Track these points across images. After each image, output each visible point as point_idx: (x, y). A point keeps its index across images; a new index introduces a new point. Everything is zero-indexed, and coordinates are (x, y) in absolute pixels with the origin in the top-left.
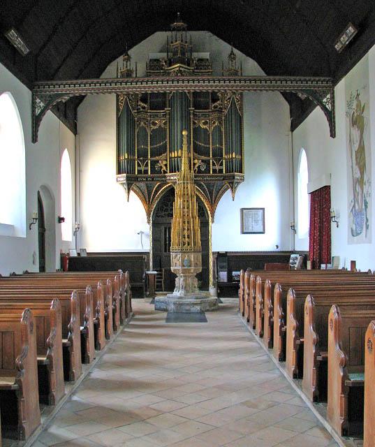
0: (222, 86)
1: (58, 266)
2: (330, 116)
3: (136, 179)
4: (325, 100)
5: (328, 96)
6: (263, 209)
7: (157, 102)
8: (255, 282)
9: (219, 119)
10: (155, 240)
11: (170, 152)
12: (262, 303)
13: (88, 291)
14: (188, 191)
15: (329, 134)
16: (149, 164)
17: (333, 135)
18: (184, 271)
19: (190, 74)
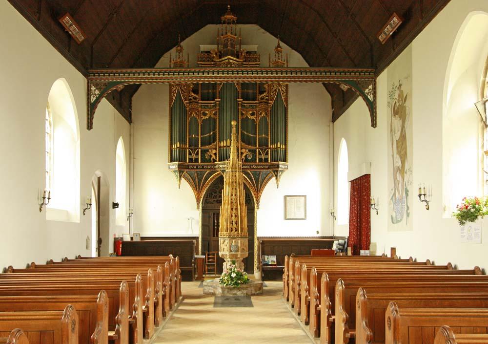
0: (270, 77)
1: (111, 250)
2: (372, 106)
3: (188, 167)
4: (367, 91)
5: (370, 87)
6: (305, 196)
7: (207, 92)
8: (300, 268)
9: (266, 110)
10: (204, 226)
11: (220, 141)
12: (308, 290)
13: (138, 279)
14: (236, 179)
15: (370, 124)
16: (200, 153)
17: (374, 125)
18: (232, 256)
19: (239, 66)
